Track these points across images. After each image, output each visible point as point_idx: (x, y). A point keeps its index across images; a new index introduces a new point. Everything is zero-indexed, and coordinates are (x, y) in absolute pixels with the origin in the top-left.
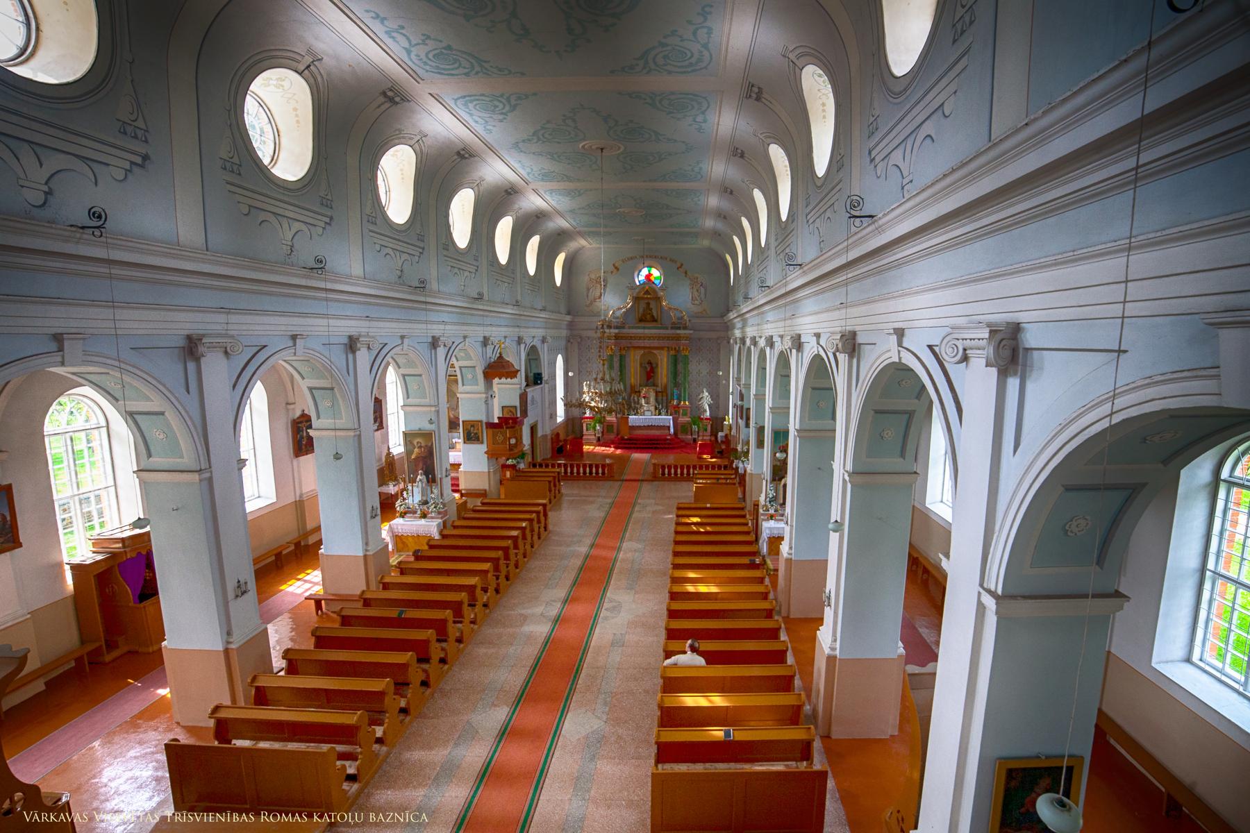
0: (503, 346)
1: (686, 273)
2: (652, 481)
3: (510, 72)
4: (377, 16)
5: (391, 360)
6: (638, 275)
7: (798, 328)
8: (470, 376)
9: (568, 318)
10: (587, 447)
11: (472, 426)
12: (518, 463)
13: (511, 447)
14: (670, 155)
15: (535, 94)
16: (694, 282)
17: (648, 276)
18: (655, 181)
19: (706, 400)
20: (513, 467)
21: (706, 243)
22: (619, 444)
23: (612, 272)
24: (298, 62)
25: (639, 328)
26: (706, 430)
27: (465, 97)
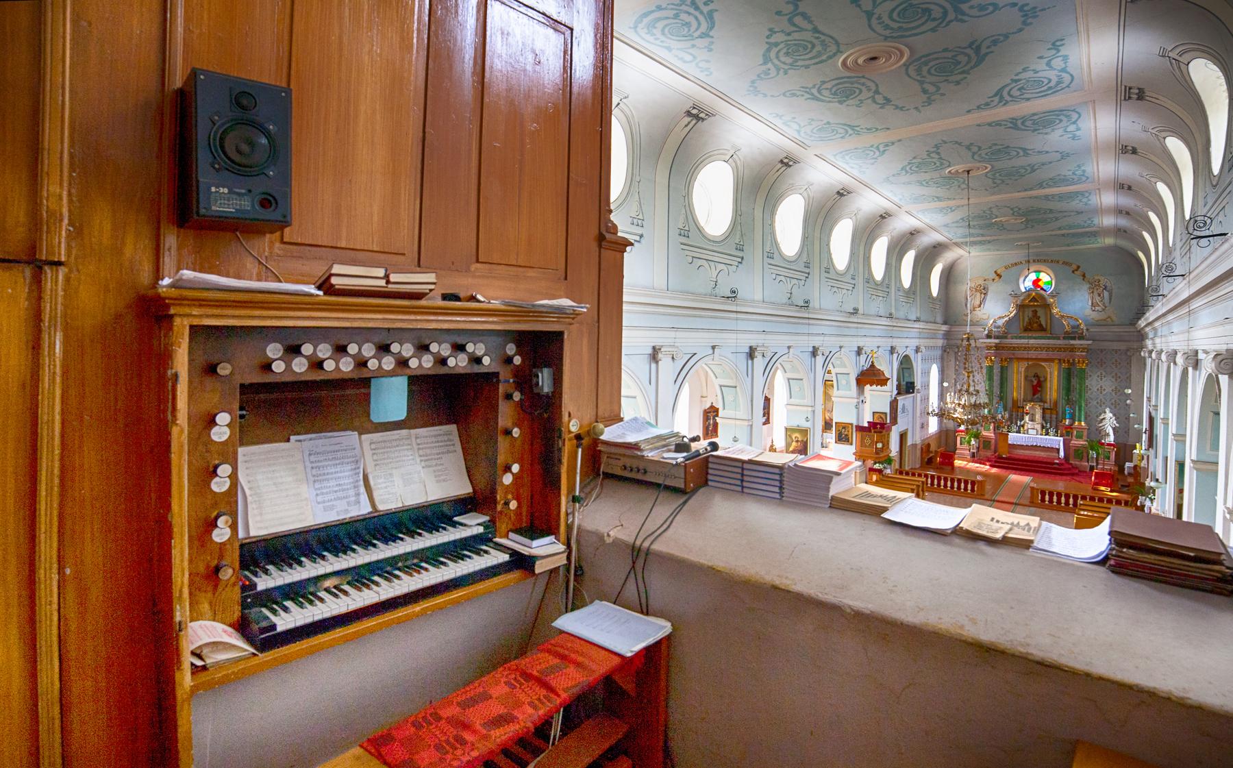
0: (875, 355)
1: (1084, 276)
2: (1030, 506)
3: (877, 129)
4: (778, 115)
5: (779, 366)
6: (1024, 280)
7: (1197, 342)
8: (844, 382)
9: (945, 328)
10: (960, 462)
11: (844, 428)
12: (885, 468)
13: (878, 451)
14: (1043, 165)
15: (900, 141)
16: (1094, 286)
17: (1036, 282)
18: (1031, 189)
19: (1109, 422)
20: (880, 471)
21: (1109, 241)
22: (996, 462)
23: (993, 280)
24: (726, 154)
25: (1024, 338)
26: (1109, 458)
27: (841, 153)
